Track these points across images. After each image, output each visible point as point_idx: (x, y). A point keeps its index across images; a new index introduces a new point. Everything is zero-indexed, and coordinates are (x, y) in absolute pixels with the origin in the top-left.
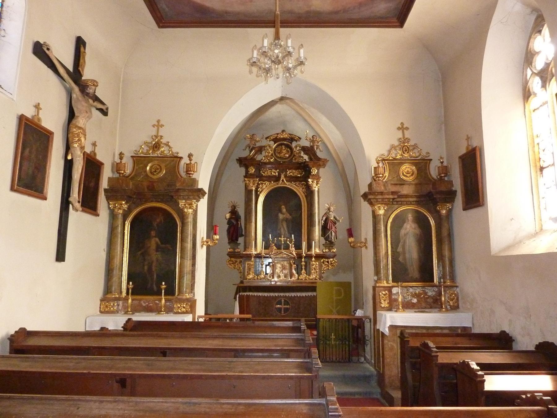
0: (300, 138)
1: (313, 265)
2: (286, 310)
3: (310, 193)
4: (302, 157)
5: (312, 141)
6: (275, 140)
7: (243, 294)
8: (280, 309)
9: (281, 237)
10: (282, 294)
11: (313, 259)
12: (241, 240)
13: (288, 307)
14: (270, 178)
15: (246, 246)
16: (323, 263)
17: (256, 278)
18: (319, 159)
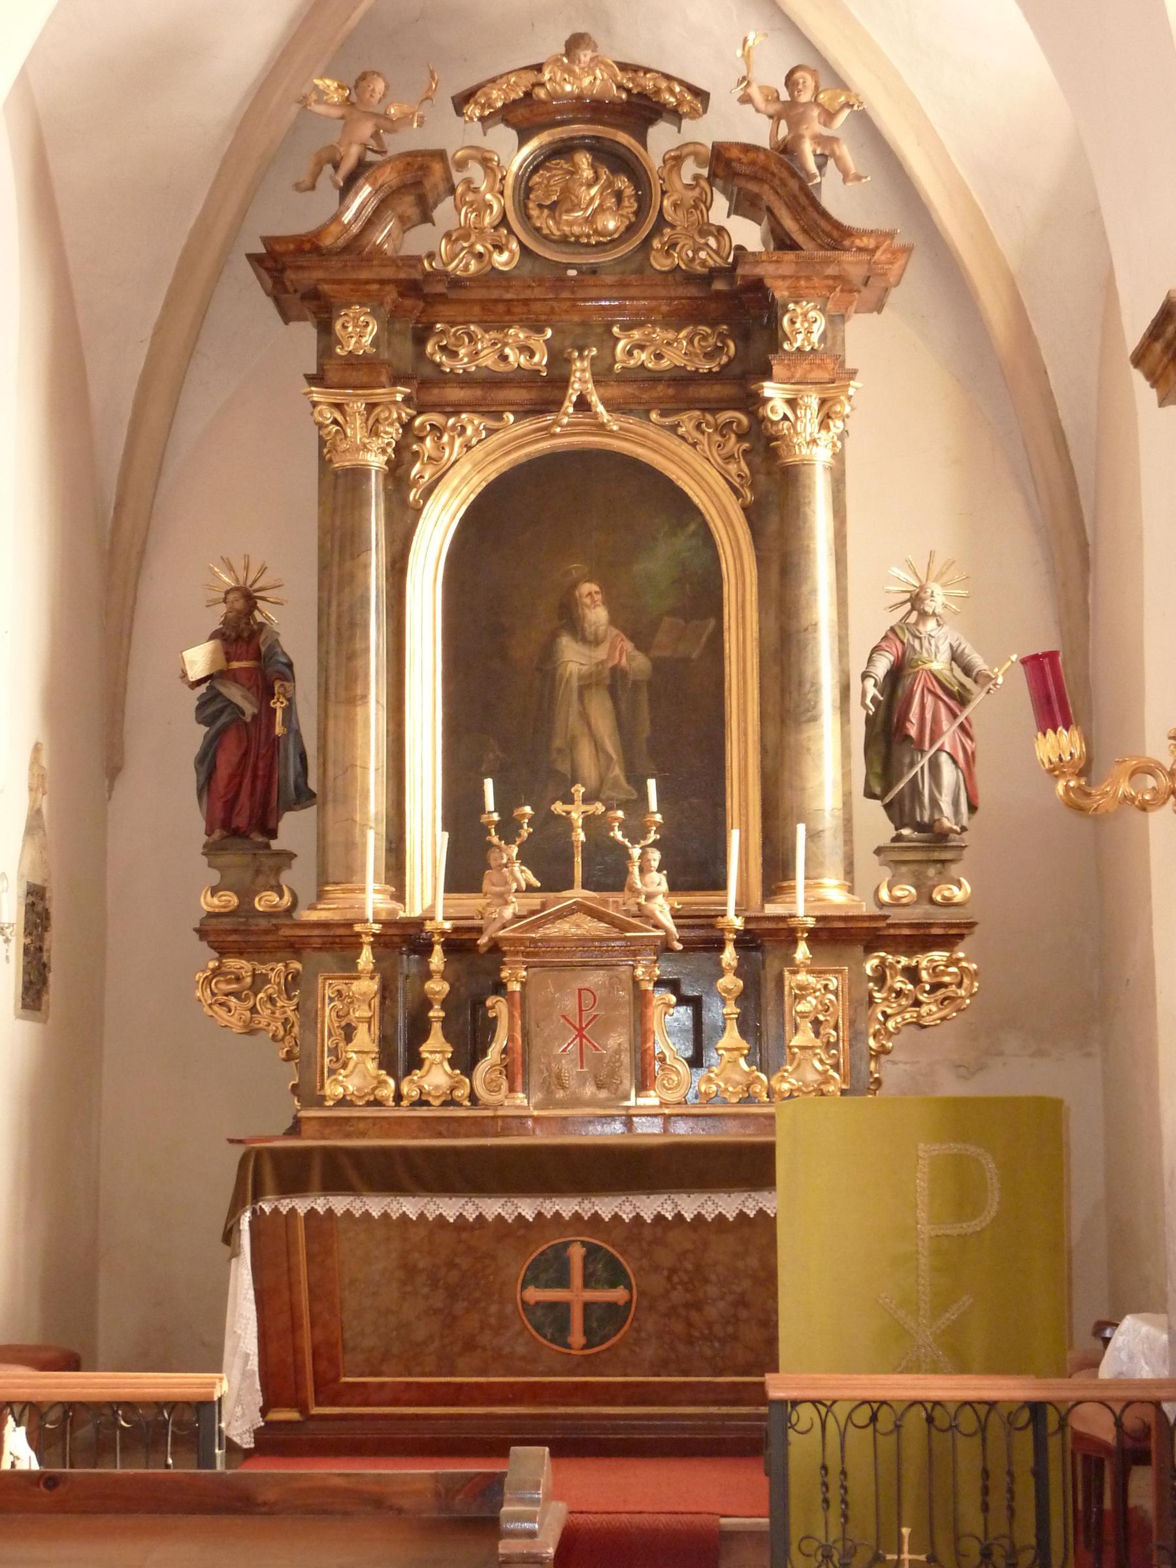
0: (702, 95)
1: (803, 991)
2: (604, 1320)
3: (772, 489)
4: (720, 231)
5: (788, 111)
6: (524, 115)
7: (285, 1205)
8: (554, 1318)
9: (569, 799)
10: (567, 1206)
11: (802, 952)
12: (294, 830)
13: (618, 1295)
14: (489, 392)
15: (334, 870)
16: (880, 979)
17: (388, 1091)
18: (836, 236)
